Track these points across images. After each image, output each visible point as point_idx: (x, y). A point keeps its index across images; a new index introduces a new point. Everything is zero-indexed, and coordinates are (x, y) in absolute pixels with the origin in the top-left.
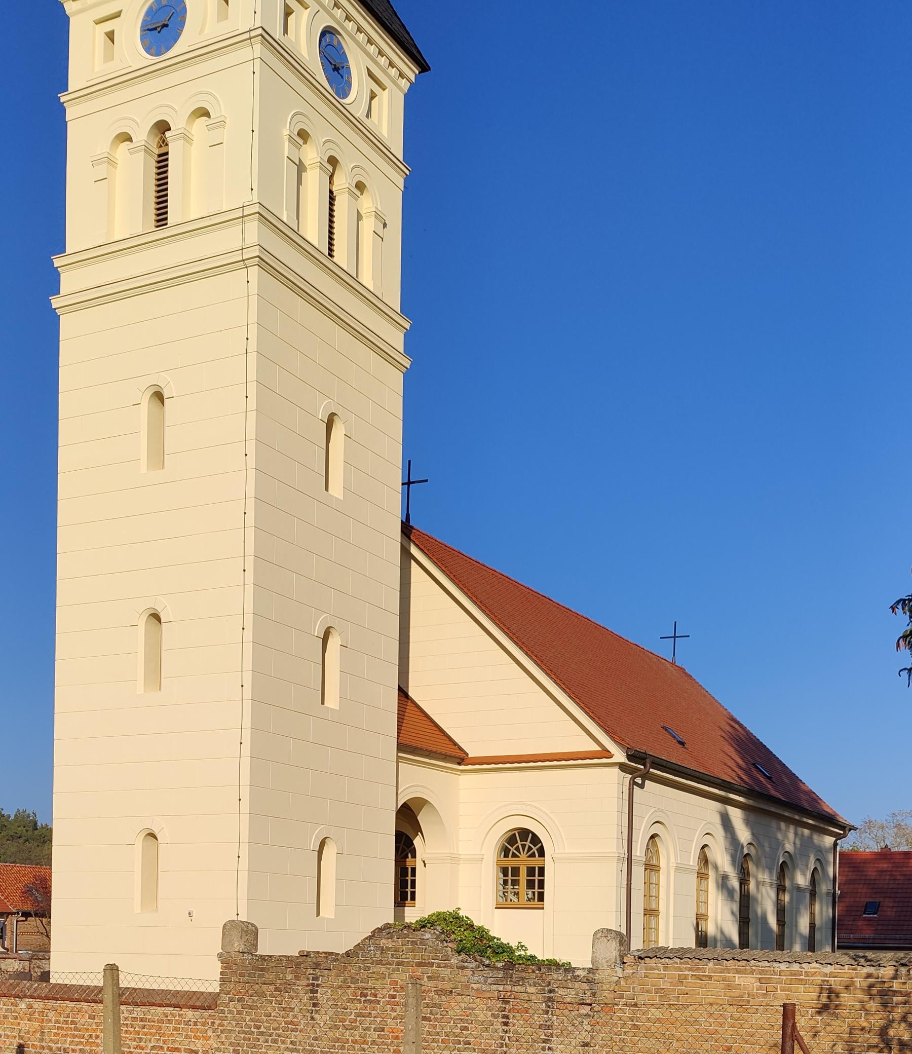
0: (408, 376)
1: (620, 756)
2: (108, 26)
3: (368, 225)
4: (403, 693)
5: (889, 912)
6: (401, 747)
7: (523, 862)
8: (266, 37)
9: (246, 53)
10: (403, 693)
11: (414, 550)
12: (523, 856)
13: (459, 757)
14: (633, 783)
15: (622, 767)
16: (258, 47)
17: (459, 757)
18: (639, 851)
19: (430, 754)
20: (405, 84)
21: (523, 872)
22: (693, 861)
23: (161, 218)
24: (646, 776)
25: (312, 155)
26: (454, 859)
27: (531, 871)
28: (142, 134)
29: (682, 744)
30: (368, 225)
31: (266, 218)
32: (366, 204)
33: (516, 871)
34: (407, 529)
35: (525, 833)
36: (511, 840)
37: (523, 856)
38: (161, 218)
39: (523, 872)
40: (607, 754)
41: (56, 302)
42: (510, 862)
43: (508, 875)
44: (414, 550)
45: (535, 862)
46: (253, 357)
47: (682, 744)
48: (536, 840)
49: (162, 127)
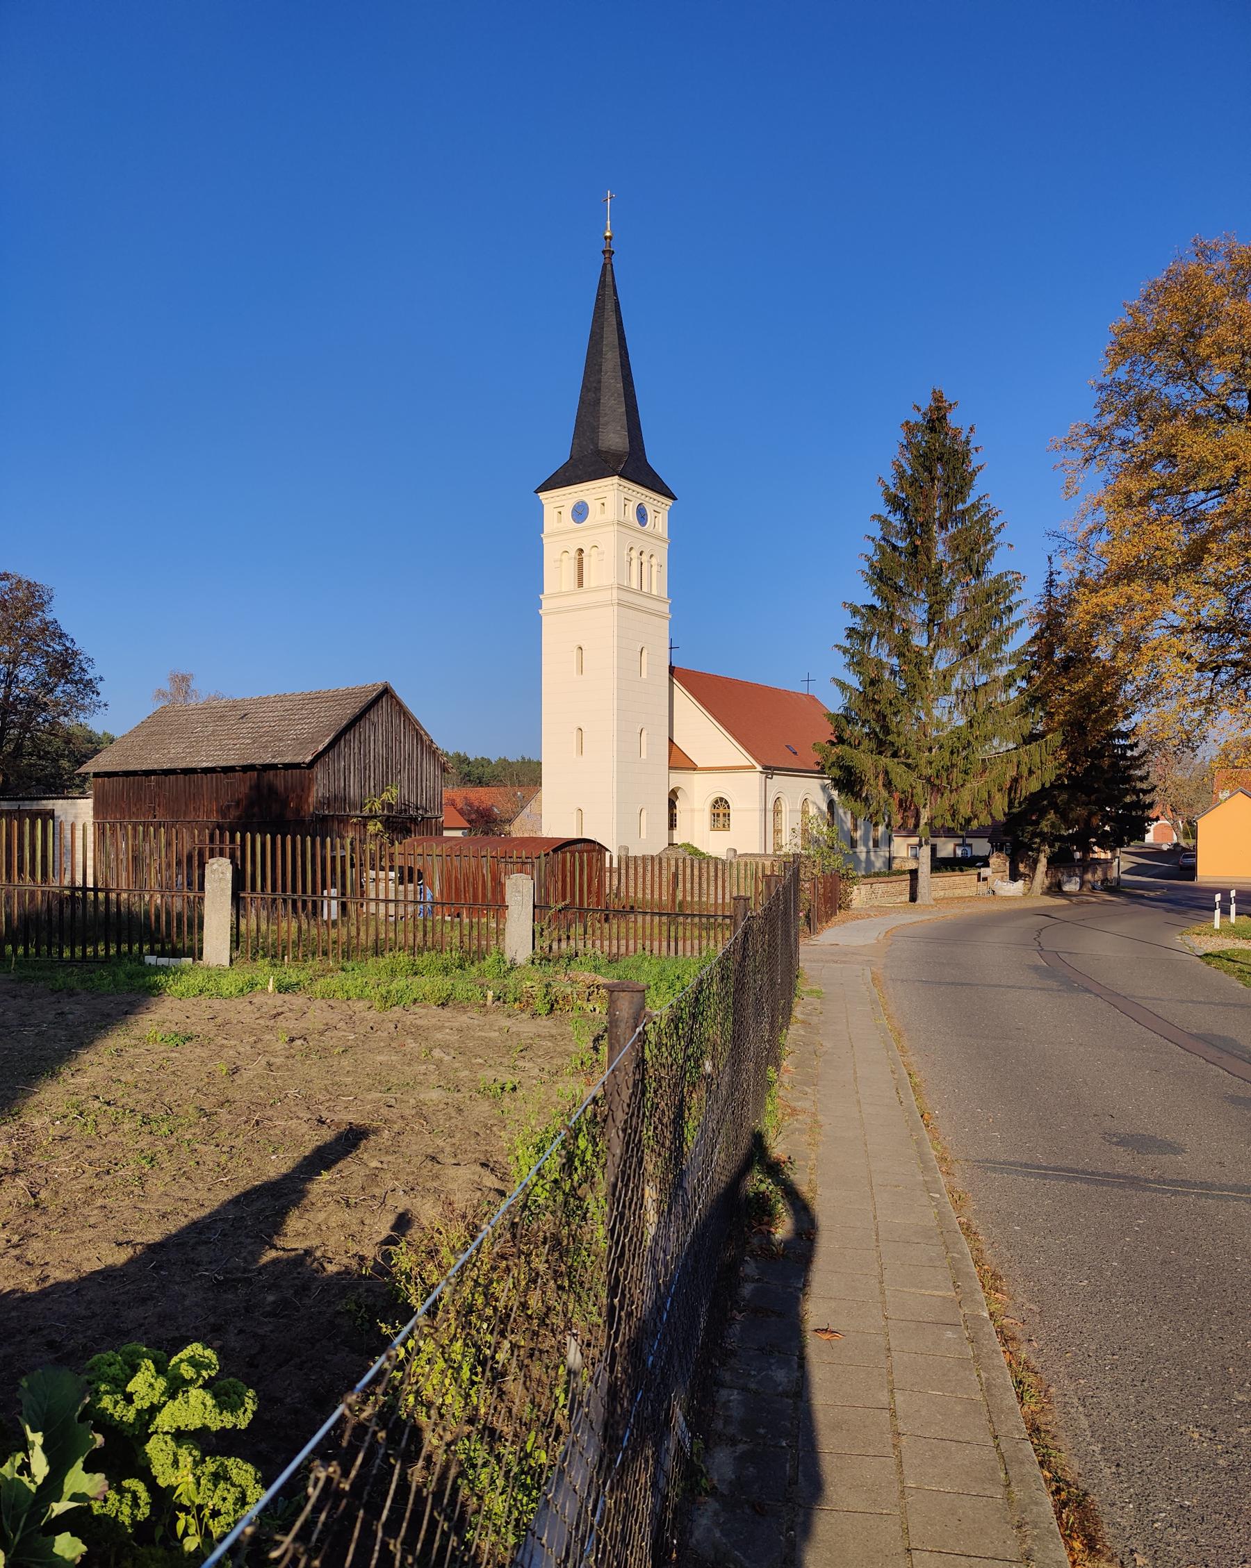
0: (671, 621)
1: (759, 768)
2: (559, 510)
3: (655, 569)
4: (671, 740)
5: (316, 932)
6: (670, 768)
7: (721, 811)
8: (619, 523)
9: (611, 528)
10: (671, 740)
11: (675, 681)
12: (721, 808)
13: (694, 768)
14: (767, 777)
15: (761, 772)
16: (616, 526)
17: (694, 768)
18: (770, 806)
19: (682, 769)
20: (668, 508)
21: (721, 815)
22: (799, 807)
23: (580, 584)
24: (773, 774)
25: (635, 554)
26: (692, 810)
27: (724, 815)
28: (573, 553)
29: (795, 753)
30: (655, 569)
31: (620, 588)
32: (654, 560)
33: (718, 815)
34: (672, 670)
35: (722, 799)
36: (716, 802)
37: (721, 808)
38: (580, 584)
39: (721, 815)
40: (754, 767)
41: (541, 612)
42: (716, 811)
43: (716, 816)
44: (675, 681)
45: (726, 811)
46: (615, 637)
47: (795, 753)
48: (726, 802)
49: (581, 551)
